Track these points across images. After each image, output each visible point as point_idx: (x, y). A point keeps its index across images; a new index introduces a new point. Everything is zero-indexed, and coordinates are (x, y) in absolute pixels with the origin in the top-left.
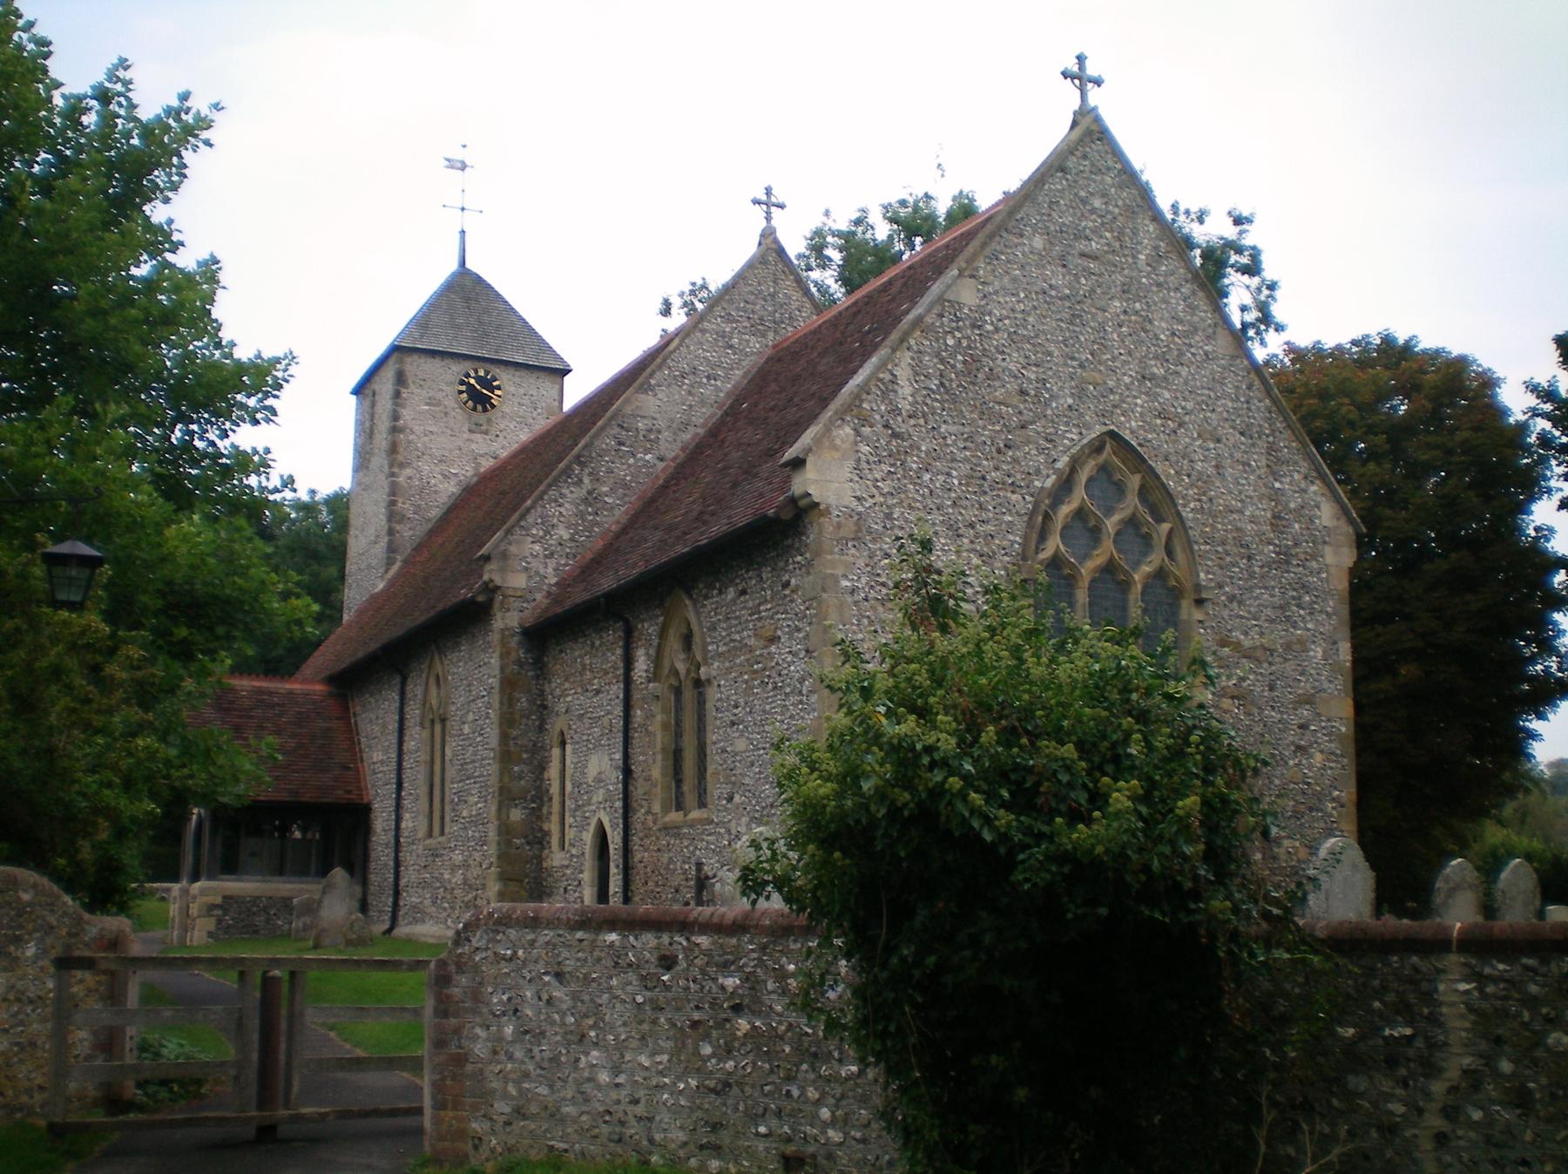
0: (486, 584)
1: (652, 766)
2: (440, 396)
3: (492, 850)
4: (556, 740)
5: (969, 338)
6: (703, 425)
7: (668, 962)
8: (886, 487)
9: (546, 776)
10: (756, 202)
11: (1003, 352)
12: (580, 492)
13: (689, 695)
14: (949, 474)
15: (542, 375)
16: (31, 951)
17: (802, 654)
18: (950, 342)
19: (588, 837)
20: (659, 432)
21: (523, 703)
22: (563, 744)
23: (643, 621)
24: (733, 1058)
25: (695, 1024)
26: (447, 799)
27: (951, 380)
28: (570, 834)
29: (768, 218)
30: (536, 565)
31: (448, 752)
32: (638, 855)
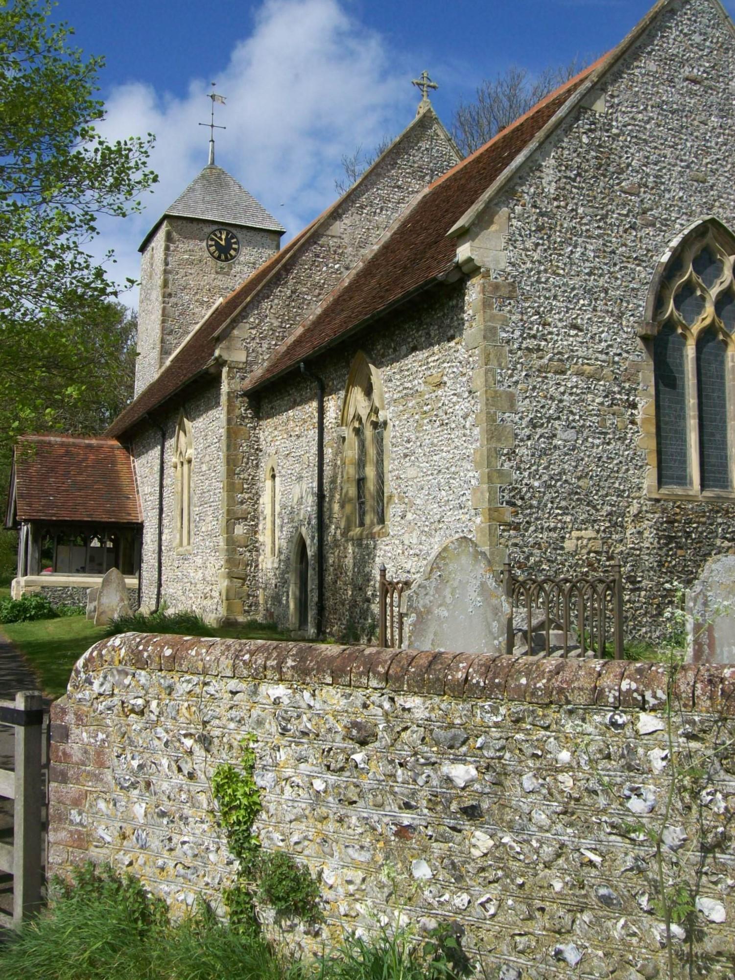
0: (216, 359)
4: (269, 475)
7: (363, 737)
13: (369, 432)
17: (466, 395)
18: (585, 140)
22: (274, 477)
23: (333, 380)
24: (467, 890)
25: (403, 832)
26: (192, 519)
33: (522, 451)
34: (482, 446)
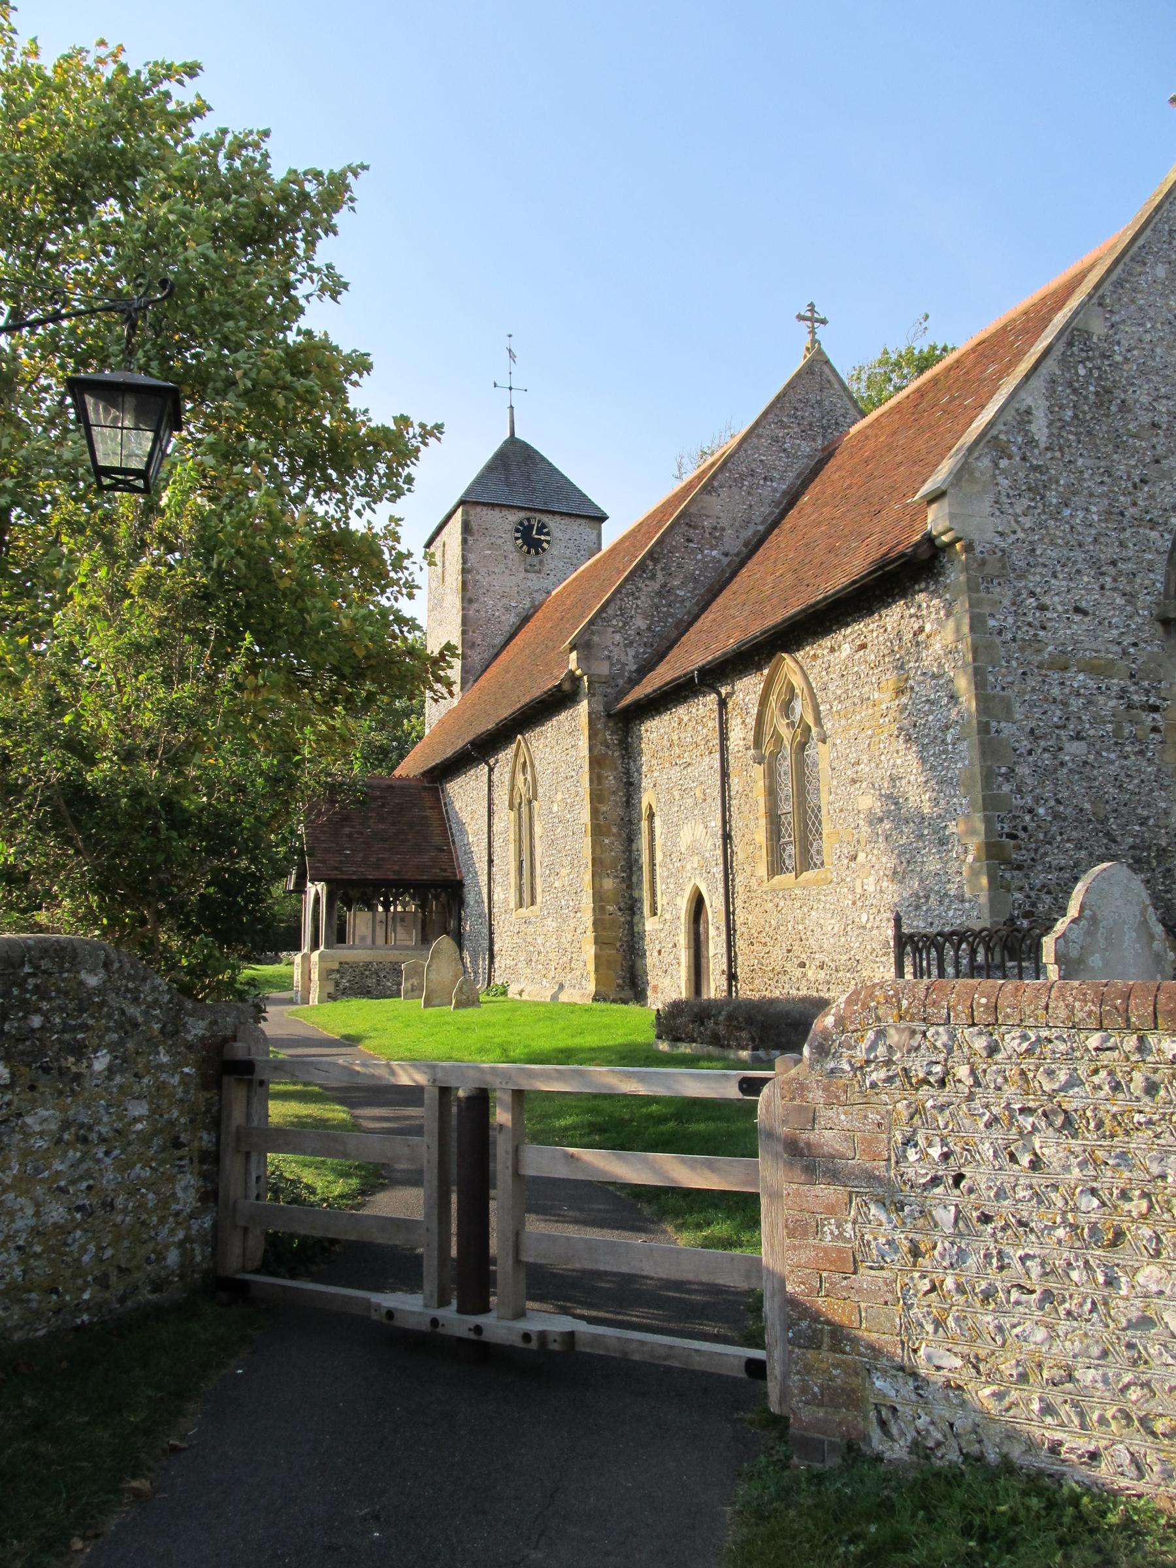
1: (752, 832)
2: (500, 542)
3: (588, 918)
5: (1099, 368)
6: (762, 523)
8: (1027, 522)
9: (634, 847)
10: (801, 318)
11: (1132, 384)
12: (656, 586)
14: (1087, 510)
15: (583, 521)
16: (101, 1063)
18: (1082, 371)
19: (683, 904)
20: (723, 529)
21: (610, 780)
22: (651, 816)
27: (1084, 413)
28: (661, 901)
29: (813, 332)
30: (616, 653)
31: (538, 830)
32: (740, 917)
33: (1023, 770)
34: (971, 764)
